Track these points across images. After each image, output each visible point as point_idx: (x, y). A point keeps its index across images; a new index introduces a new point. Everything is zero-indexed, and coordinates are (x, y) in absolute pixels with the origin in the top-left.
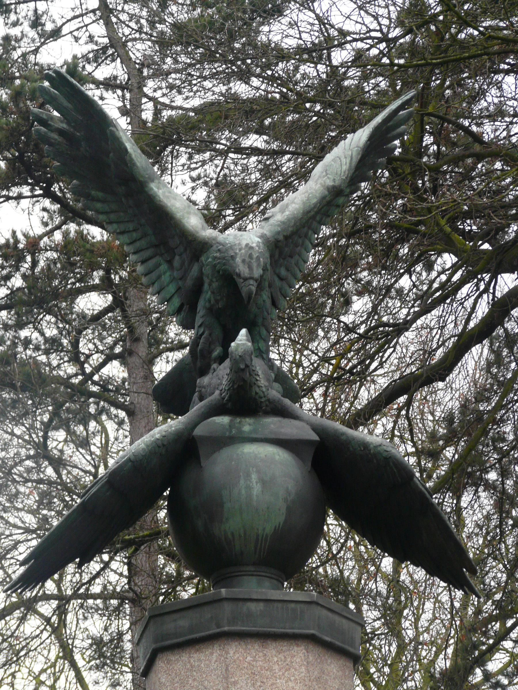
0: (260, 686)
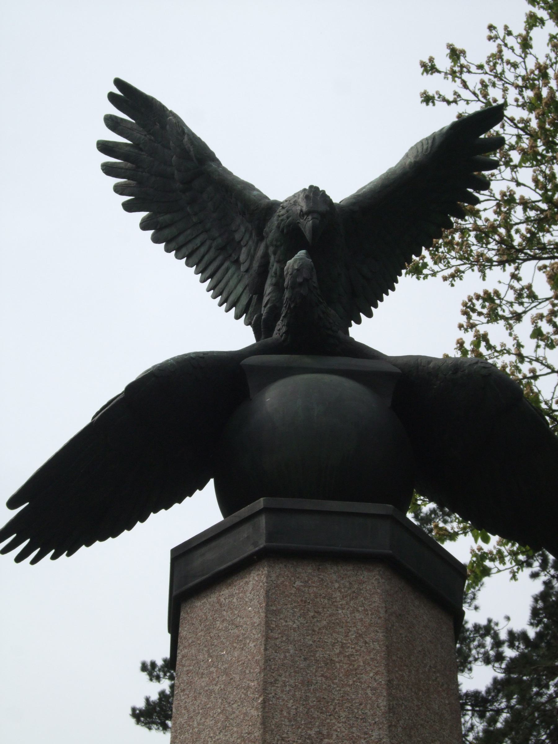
0: (313, 617)
